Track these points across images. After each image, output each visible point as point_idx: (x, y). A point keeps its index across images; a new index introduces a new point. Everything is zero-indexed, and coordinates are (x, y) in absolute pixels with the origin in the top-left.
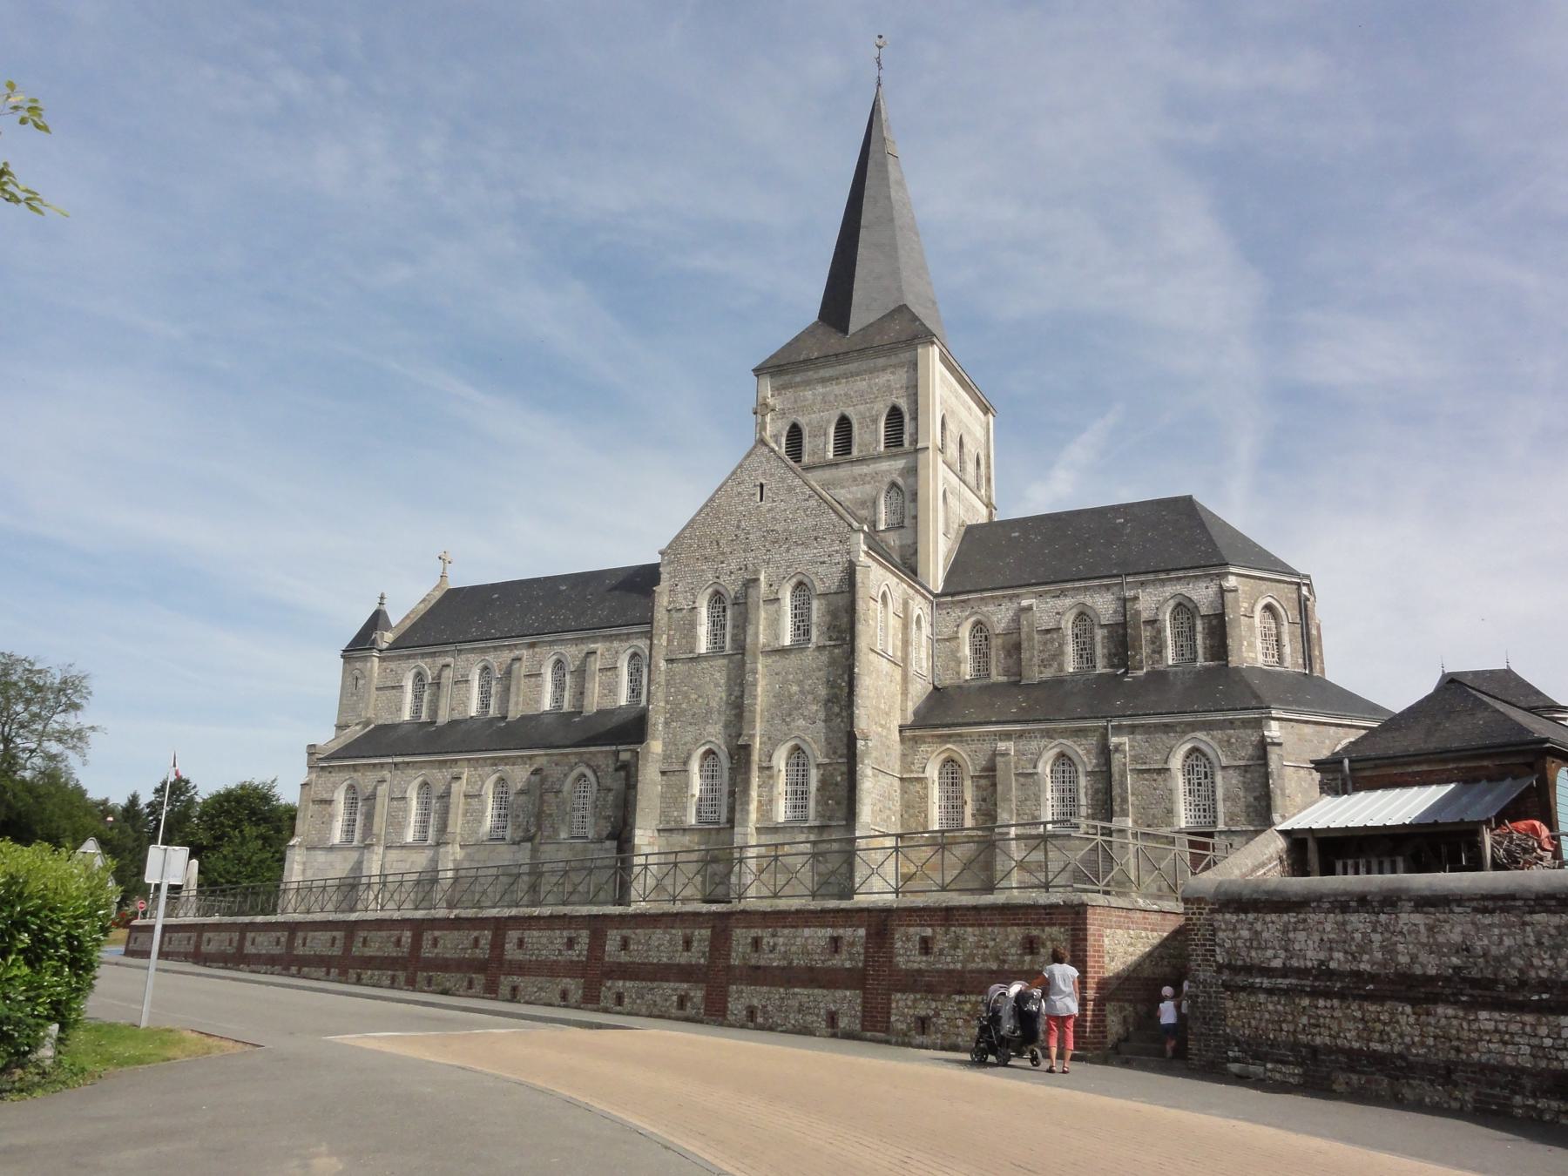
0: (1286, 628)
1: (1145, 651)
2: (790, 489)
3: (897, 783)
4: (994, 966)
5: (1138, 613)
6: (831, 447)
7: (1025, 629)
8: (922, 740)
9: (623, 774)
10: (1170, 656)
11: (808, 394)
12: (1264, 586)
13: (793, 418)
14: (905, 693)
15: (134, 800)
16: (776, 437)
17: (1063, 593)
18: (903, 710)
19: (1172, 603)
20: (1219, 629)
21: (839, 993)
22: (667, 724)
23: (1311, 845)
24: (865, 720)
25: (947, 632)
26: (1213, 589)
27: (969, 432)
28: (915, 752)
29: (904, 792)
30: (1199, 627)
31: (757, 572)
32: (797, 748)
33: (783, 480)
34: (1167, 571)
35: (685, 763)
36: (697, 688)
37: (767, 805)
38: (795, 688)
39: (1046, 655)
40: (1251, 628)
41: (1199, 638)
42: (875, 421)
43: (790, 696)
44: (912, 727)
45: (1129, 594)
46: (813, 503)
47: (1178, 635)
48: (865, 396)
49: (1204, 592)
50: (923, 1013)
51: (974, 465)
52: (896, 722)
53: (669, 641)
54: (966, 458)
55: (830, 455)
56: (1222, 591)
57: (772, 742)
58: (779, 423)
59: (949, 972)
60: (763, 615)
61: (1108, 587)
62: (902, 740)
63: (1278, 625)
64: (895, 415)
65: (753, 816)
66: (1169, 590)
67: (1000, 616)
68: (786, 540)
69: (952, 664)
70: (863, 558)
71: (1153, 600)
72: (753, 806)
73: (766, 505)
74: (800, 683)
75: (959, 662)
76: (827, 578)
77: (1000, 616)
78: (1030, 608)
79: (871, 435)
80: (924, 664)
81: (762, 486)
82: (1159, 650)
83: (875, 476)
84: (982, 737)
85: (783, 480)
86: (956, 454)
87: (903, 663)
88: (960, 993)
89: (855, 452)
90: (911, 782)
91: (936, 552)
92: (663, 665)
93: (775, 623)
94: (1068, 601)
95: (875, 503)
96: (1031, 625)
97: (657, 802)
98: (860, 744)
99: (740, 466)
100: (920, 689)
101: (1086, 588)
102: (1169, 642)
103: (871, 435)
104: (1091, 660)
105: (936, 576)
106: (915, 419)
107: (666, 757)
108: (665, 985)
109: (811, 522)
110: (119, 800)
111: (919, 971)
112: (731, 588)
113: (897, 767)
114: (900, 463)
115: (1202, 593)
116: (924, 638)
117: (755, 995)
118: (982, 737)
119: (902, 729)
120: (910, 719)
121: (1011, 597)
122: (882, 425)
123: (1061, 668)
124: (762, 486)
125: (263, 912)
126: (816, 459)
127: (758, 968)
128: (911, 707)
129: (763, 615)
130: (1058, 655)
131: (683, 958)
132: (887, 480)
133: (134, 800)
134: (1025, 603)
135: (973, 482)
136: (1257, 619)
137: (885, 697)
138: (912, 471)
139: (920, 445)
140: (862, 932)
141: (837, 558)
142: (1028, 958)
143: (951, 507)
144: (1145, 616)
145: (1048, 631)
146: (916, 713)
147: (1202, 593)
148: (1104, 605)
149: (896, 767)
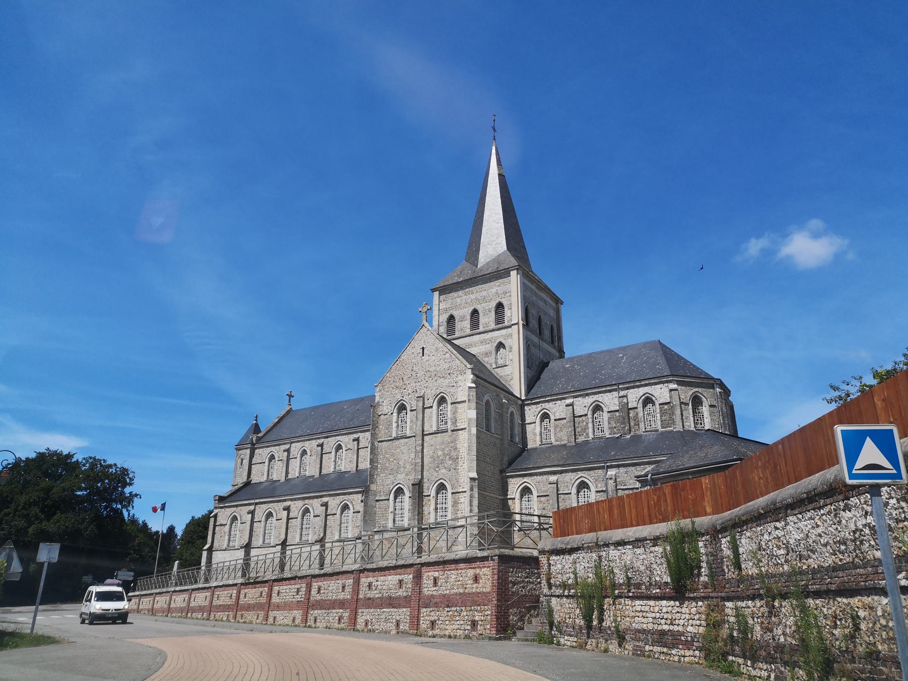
4: (462, 591)
11: (458, 300)
15: (171, 529)
21: (401, 610)
23: (647, 518)
27: (546, 314)
33: (433, 345)
34: (640, 381)
36: (393, 455)
38: (440, 453)
43: (438, 457)
46: (448, 356)
50: (433, 619)
54: (543, 327)
59: (444, 596)
73: (426, 358)
79: (487, 320)
81: (423, 348)
86: (536, 326)
88: (448, 606)
89: (481, 329)
103: (487, 320)
108: (334, 611)
109: (446, 366)
110: (154, 530)
111: (432, 596)
121: (561, 399)
124: (423, 348)
125: (191, 583)
127: (370, 599)
131: (341, 596)
133: (171, 529)
135: (549, 340)
140: (411, 576)
142: (475, 585)
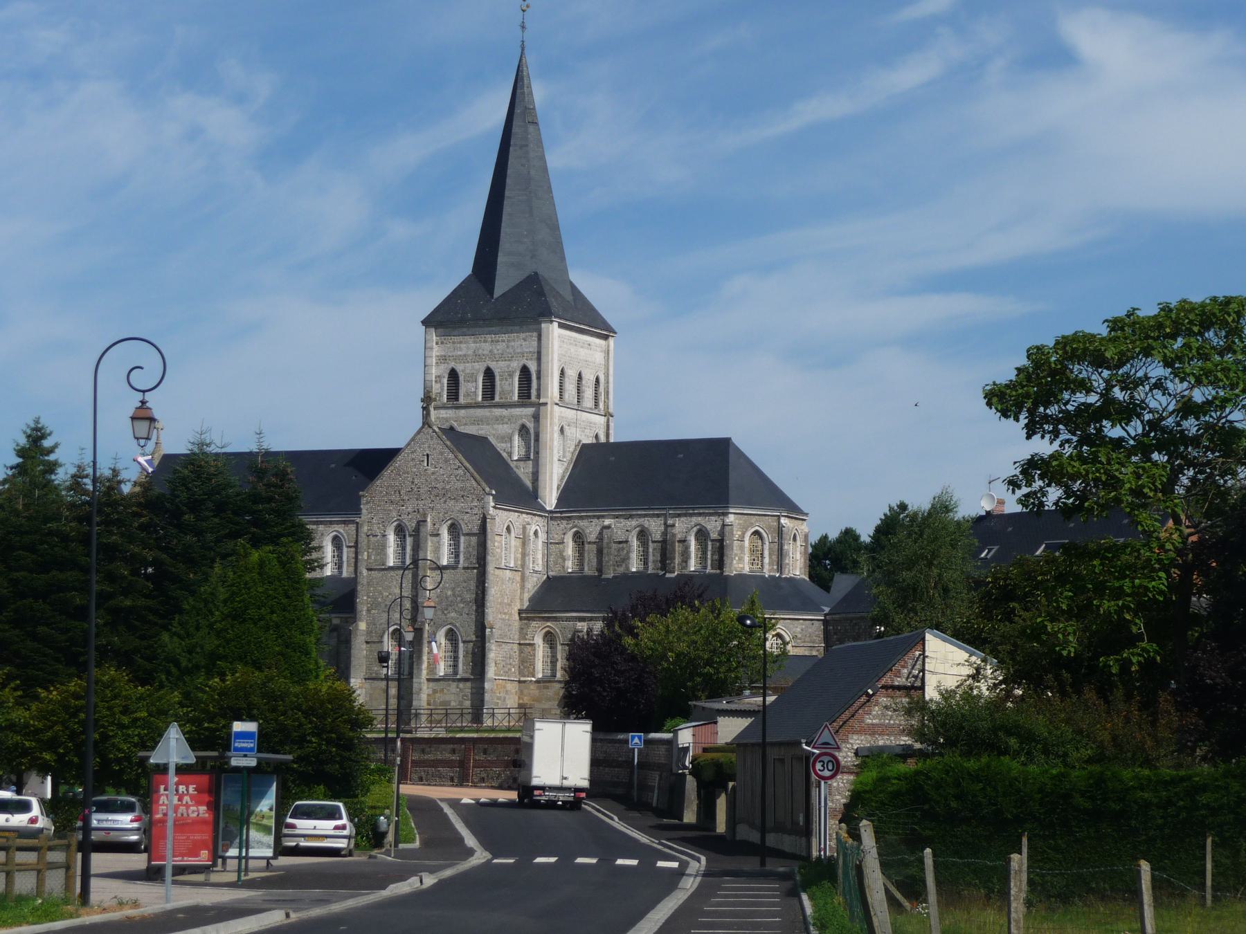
0: (766, 547)
1: (677, 560)
2: (446, 461)
3: (516, 647)
5: (674, 535)
6: (480, 393)
7: (606, 541)
8: (533, 619)
9: (335, 634)
10: (693, 566)
12: (754, 519)
13: (452, 364)
14: (523, 587)
16: (439, 377)
17: (631, 516)
18: (521, 600)
19: (695, 529)
20: (721, 549)
22: (368, 611)
24: (491, 615)
25: (557, 538)
26: (719, 524)
28: (528, 626)
29: (521, 652)
30: (710, 548)
31: (425, 515)
32: (451, 630)
35: (382, 637)
37: (432, 667)
39: (618, 559)
40: (742, 548)
41: (709, 553)
42: (511, 375)
44: (526, 611)
45: (670, 522)
46: (460, 472)
47: (697, 550)
48: (502, 351)
49: (713, 524)
51: (591, 387)
52: (517, 606)
53: (369, 556)
55: (480, 399)
56: (724, 525)
57: (437, 626)
58: (442, 367)
60: (430, 544)
61: (658, 516)
62: (521, 619)
63: (763, 543)
64: (525, 371)
65: (424, 672)
66: (695, 520)
67: (592, 530)
68: (444, 495)
69: (560, 560)
70: (492, 511)
71: (683, 526)
72: (425, 665)
74: (453, 589)
75: (564, 560)
76: (470, 524)
77: (592, 530)
78: (609, 527)
79: (509, 387)
80: (540, 562)
82: (685, 560)
83: (510, 419)
84: (568, 619)
85: (442, 454)
87: (521, 569)
90: (526, 646)
91: (551, 479)
92: (365, 572)
93: (437, 549)
94: (634, 523)
95: (511, 440)
96: (610, 538)
97: (364, 661)
98: (488, 630)
99: (413, 439)
100: (533, 584)
101: (645, 516)
102: (693, 555)
104: (646, 563)
105: (550, 498)
106: (539, 378)
107: (369, 632)
109: (459, 485)
112: (410, 525)
113: (516, 637)
114: (530, 411)
115: (712, 525)
116: (540, 544)
117: (421, 771)
118: (568, 619)
119: (520, 612)
120: (526, 604)
121: (599, 517)
122: (516, 379)
123: (628, 568)
126: (469, 401)
128: (527, 596)
129: (430, 544)
130: (626, 559)
132: (520, 422)
134: (607, 522)
136: (747, 543)
137: (508, 593)
138: (536, 418)
139: (542, 401)
141: (476, 510)
143: (566, 432)
144: (679, 537)
145: (620, 542)
146: (530, 600)
147: (712, 525)
148: (655, 527)
149: (516, 637)
